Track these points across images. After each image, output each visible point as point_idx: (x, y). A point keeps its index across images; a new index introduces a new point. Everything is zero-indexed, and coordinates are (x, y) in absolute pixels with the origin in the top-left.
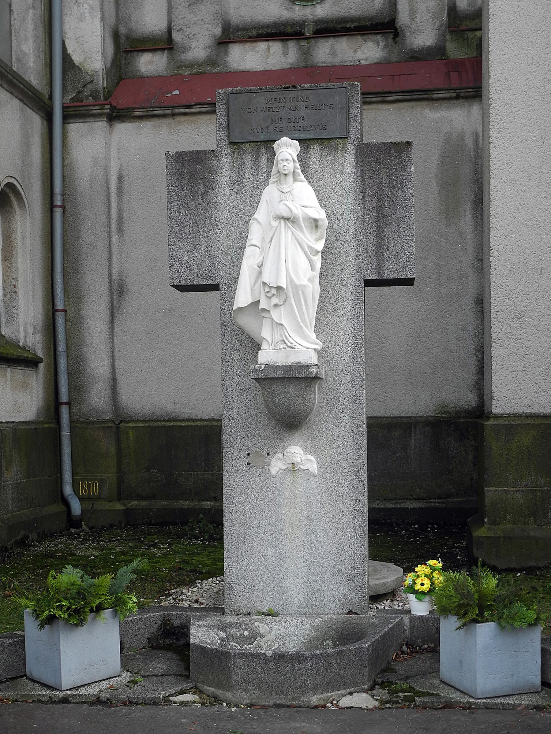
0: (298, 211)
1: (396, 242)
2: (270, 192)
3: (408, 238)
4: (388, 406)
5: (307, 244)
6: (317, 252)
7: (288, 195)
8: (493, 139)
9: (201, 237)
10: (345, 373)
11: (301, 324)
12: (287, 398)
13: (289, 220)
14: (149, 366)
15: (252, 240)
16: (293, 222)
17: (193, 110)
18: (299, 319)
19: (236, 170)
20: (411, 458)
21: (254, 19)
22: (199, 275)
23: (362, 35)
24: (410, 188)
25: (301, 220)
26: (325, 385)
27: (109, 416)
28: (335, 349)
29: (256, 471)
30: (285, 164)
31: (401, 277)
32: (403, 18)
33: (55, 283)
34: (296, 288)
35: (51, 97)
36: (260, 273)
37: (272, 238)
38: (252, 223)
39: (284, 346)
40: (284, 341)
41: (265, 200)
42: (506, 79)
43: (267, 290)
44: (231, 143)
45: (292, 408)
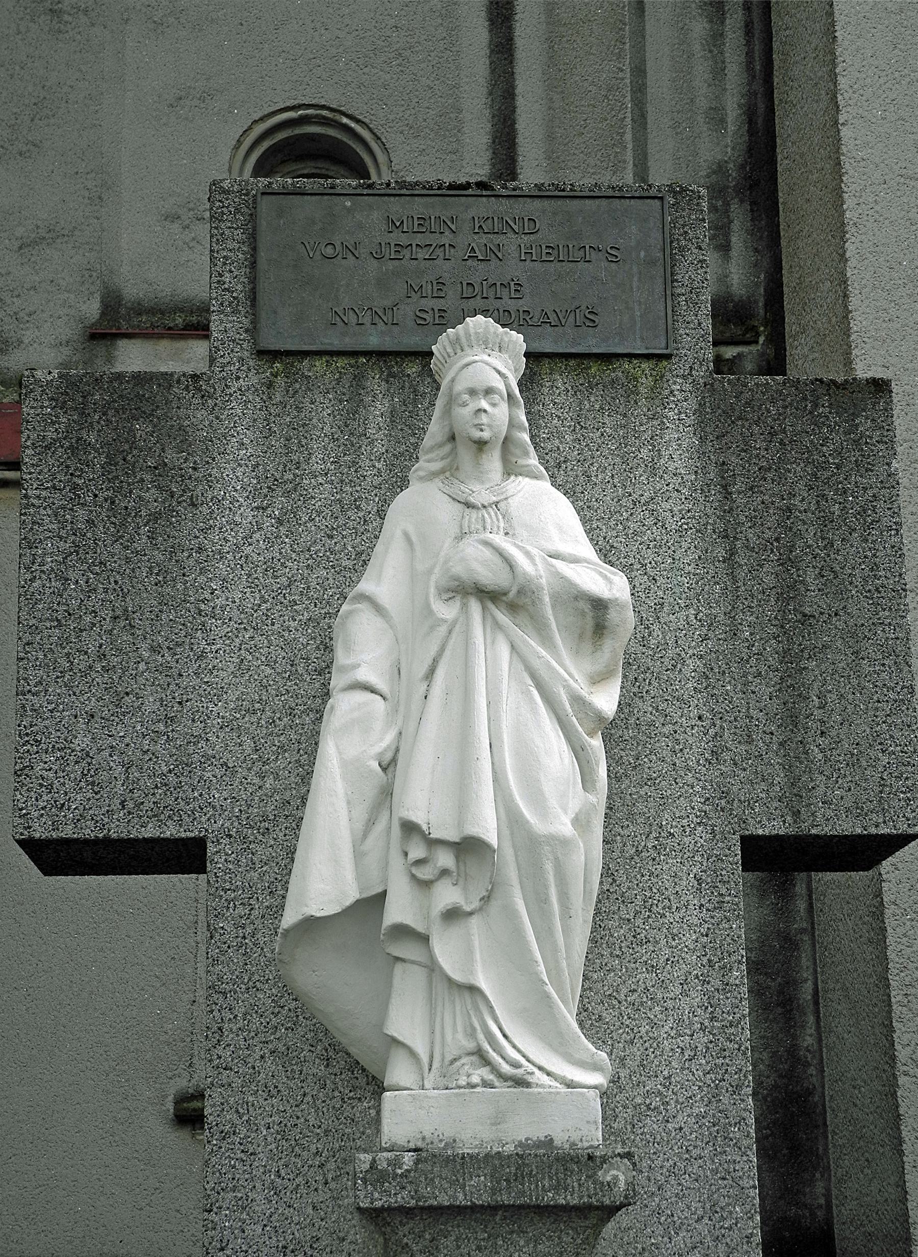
1: (850, 709)
2: (421, 508)
3: (892, 695)
5: (567, 687)
7: (490, 516)
9: (142, 666)
11: (550, 989)
13: (503, 598)
15: (356, 666)
19: (277, 443)
21: (178, 292)
22: (130, 805)
25: (547, 599)
28: (642, 1090)
31: (873, 831)
34: (532, 846)
38: (350, 613)
39: (484, 1073)
40: (480, 1053)
41: (399, 533)
43: (417, 851)
44: (261, 353)
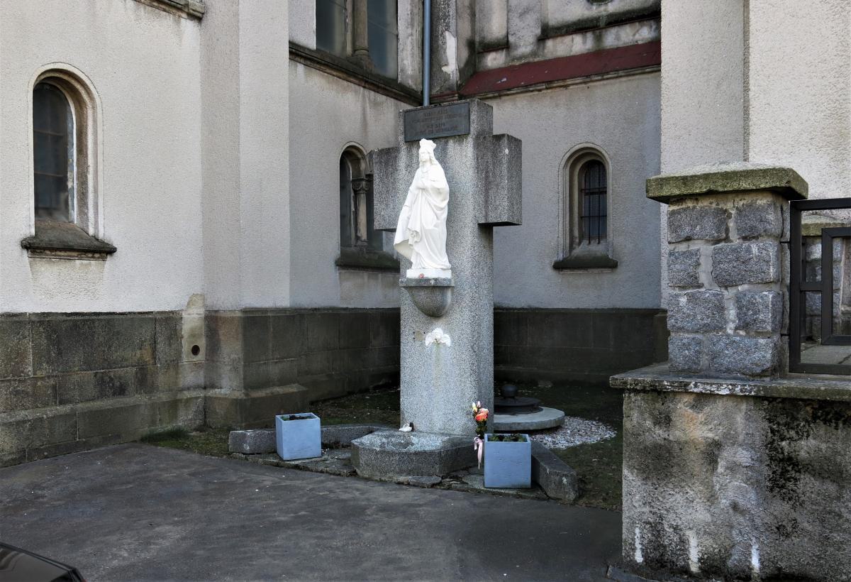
8: (663, 107)
12: (434, 301)
17: (512, 92)
23: (639, 22)
29: (418, 343)
33: (359, 221)
35: (422, 92)
42: (673, 61)
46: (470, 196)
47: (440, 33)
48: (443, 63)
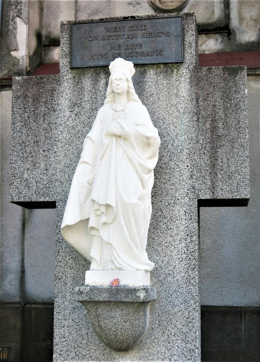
0: (129, 129)
3: (242, 159)
4: (224, 298)
6: (151, 171)
9: (41, 155)
10: (178, 294)
11: (131, 244)
14: (49, 263)
16: (125, 139)
18: (129, 238)
20: (242, 339)
22: (37, 192)
23: (206, 34)
24: (244, 110)
25: (133, 137)
26: (157, 306)
27: (17, 299)
28: (167, 269)
30: (119, 83)
31: (235, 197)
32: (234, 22)
36: (90, 191)
37: (103, 155)
40: (112, 261)
43: (96, 207)
45: (120, 333)
46: (184, 156)
47: (11, 18)
48: (12, 47)
